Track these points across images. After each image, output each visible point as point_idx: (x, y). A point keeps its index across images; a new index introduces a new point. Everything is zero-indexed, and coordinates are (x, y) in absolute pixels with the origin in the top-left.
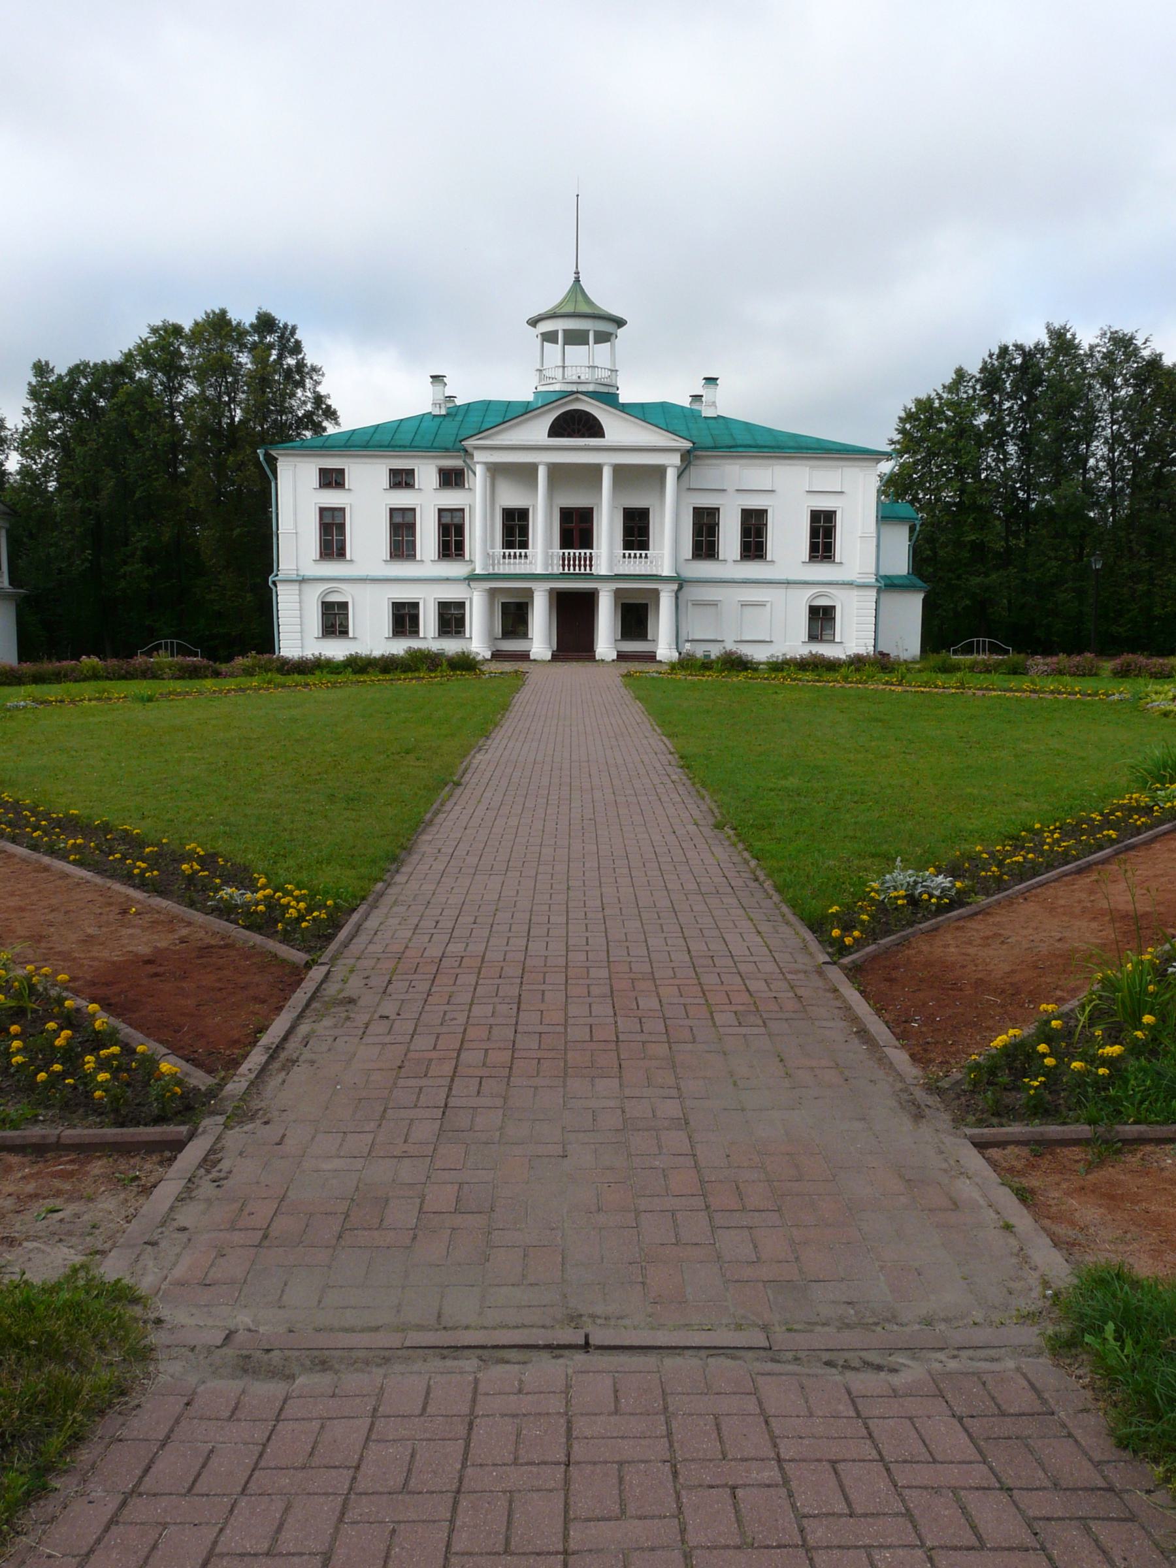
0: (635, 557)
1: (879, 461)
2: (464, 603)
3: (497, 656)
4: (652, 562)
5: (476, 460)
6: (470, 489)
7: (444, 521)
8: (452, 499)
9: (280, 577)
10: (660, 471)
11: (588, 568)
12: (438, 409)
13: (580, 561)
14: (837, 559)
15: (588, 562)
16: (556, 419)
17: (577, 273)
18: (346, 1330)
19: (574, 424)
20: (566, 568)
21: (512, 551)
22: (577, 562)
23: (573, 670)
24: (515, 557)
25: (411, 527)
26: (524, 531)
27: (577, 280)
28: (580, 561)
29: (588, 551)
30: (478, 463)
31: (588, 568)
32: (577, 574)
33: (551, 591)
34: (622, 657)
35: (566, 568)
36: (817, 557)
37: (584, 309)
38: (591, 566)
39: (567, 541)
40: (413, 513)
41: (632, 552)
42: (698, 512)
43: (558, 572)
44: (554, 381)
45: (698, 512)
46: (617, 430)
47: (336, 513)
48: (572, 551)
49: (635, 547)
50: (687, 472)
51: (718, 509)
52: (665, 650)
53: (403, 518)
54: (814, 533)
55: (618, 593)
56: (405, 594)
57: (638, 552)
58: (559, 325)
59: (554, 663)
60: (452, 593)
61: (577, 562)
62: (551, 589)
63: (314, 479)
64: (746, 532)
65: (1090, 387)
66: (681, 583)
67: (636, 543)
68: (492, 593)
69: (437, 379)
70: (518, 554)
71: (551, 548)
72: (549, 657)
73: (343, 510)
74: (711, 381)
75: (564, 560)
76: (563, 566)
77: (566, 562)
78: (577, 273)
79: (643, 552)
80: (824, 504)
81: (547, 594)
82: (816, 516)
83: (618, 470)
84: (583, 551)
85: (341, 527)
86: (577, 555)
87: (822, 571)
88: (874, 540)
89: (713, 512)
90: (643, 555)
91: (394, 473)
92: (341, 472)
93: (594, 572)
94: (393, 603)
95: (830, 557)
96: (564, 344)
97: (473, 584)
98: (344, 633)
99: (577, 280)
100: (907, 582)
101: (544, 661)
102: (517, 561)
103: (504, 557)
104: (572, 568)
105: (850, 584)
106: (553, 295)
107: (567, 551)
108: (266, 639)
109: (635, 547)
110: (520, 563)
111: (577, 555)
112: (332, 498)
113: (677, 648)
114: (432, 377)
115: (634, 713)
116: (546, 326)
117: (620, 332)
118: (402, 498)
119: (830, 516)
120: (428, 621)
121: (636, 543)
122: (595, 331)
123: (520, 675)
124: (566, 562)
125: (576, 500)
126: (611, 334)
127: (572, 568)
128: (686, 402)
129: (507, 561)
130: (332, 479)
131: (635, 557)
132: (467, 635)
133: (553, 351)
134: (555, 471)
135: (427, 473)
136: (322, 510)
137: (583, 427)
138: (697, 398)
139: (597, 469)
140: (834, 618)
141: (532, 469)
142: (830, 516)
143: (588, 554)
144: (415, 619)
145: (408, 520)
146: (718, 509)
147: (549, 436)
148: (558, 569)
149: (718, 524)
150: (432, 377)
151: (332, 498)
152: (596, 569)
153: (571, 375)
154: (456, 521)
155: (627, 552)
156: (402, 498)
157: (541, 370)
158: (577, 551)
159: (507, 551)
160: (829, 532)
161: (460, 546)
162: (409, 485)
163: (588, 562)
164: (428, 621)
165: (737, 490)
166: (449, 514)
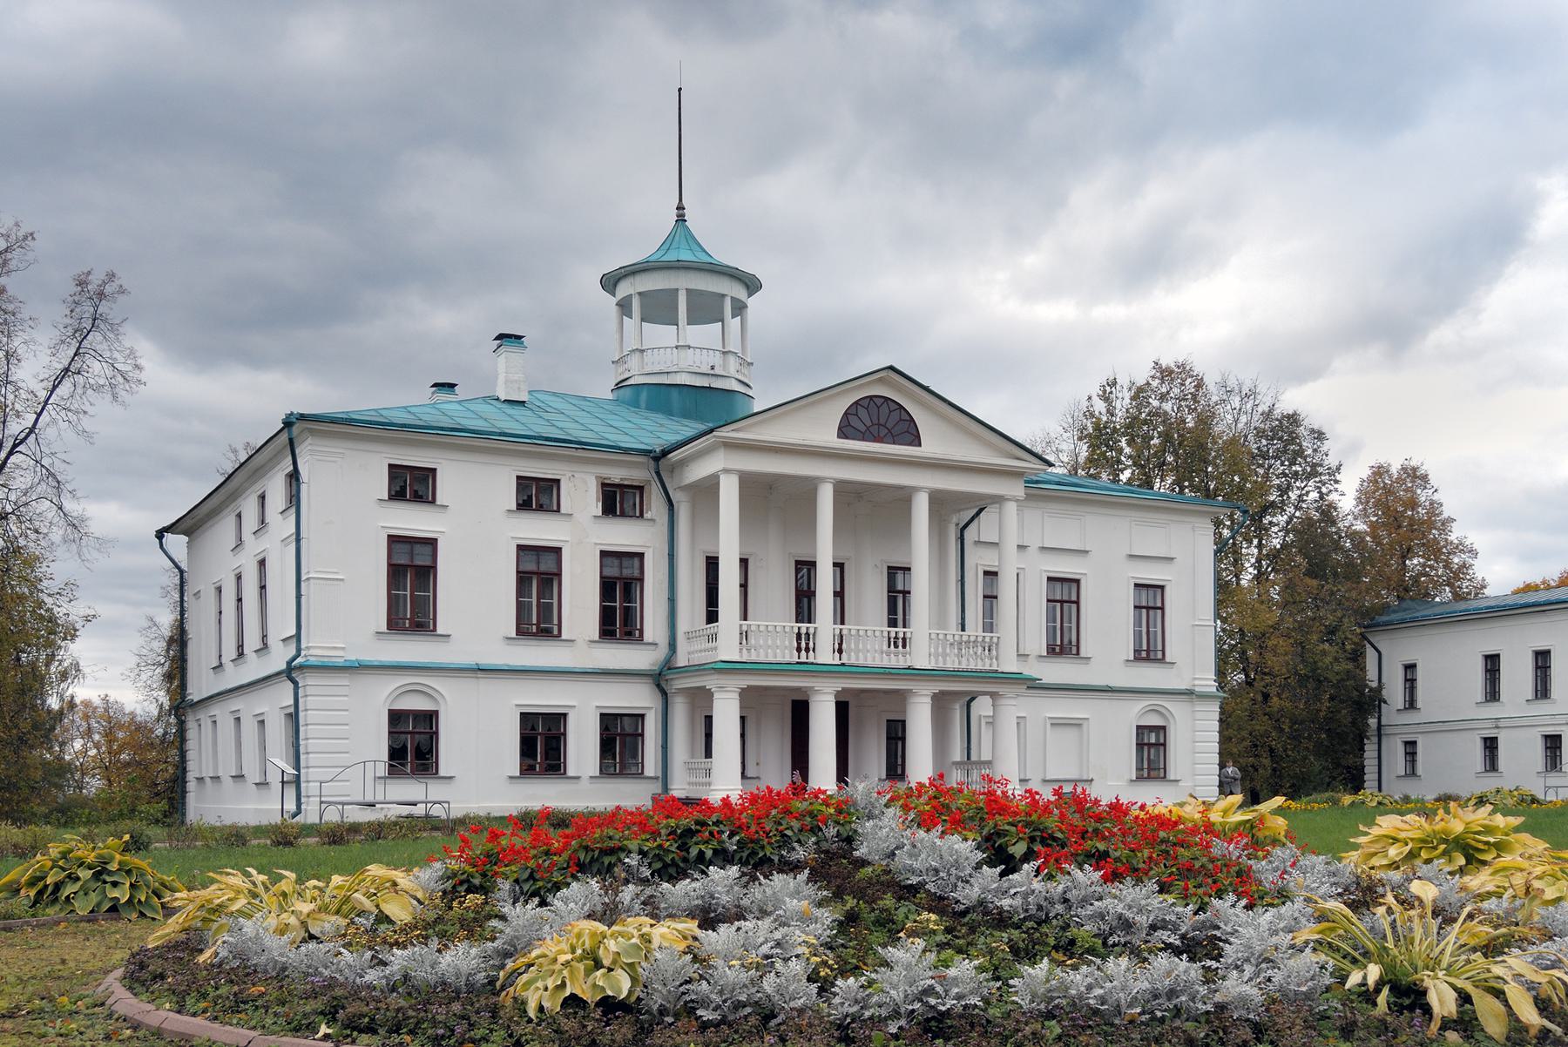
7: (605, 574)
8: (622, 535)
17: (680, 208)
27: (681, 219)
37: (686, 256)
43: (788, 659)
46: (935, 441)
53: (538, 563)
56: (544, 698)
63: (380, 484)
71: (895, 626)
73: (432, 543)
76: (799, 650)
78: (680, 208)
80: (1151, 574)
87: (1148, 676)
91: (523, 482)
99: (681, 219)
105: (1189, 693)
112: (412, 520)
118: (539, 530)
132: (899, 772)
134: (848, 494)
136: (394, 540)
143: (901, 635)
145: (547, 565)
147: (842, 433)
148: (791, 657)
151: (412, 520)
154: (626, 573)
156: (539, 530)
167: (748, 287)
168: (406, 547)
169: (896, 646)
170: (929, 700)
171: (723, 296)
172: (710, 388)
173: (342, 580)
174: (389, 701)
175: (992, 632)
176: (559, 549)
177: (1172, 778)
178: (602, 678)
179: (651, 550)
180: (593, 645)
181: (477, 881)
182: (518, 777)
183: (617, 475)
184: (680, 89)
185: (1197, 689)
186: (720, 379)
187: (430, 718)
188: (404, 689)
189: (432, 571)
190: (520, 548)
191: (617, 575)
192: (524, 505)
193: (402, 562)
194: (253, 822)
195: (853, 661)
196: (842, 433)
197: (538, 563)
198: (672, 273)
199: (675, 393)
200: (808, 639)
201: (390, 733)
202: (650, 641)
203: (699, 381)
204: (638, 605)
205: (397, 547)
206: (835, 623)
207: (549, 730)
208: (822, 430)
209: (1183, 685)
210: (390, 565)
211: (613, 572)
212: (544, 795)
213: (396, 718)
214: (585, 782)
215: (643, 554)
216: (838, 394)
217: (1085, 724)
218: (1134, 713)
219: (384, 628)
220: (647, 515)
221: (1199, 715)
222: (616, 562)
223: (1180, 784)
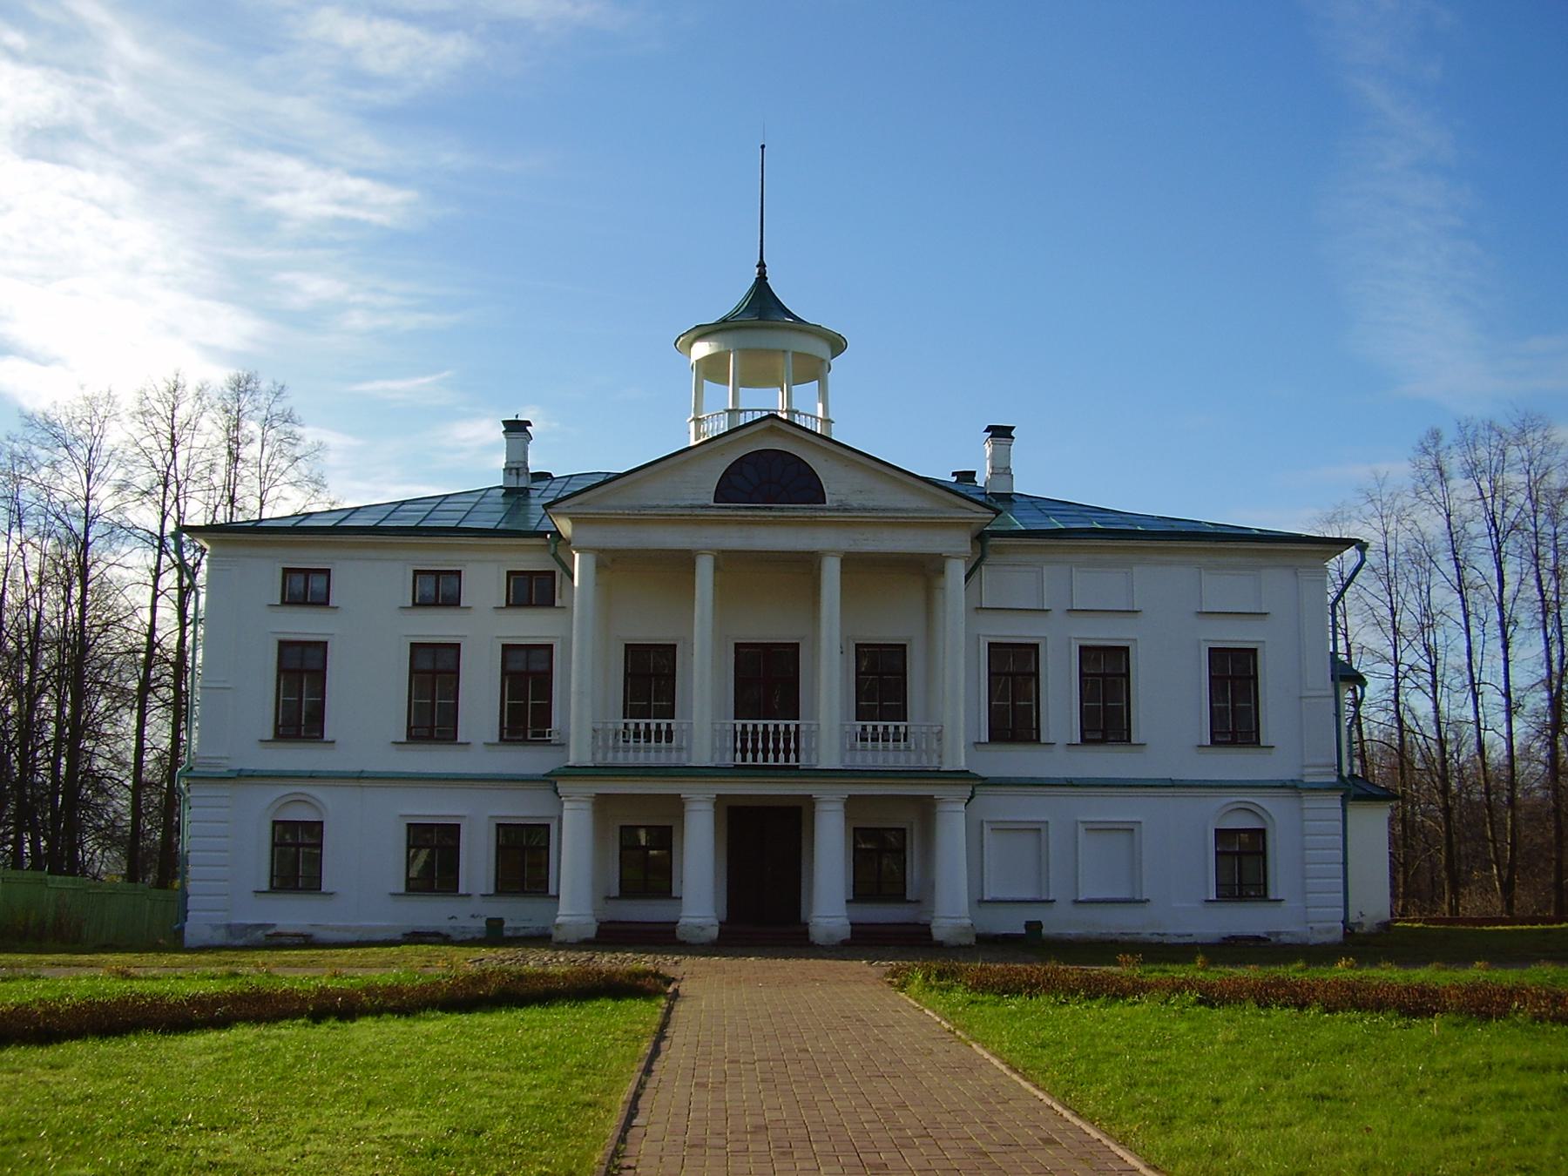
2: (548, 826)
7: (511, 666)
8: (529, 626)
12: (514, 478)
17: (762, 265)
18: (702, 507)
27: (762, 278)
29: (792, 724)
32: (782, 767)
43: (731, 764)
56: (434, 807)
60: (521, 807)
63: (273, 589)
68: (602, 803)
74: (1001, 433)
76: (744, 751)
78: (762, 265)
80: (1234, 635)
85: (320, 674)
87: (1235, 764)
88: (1332, 700)
89: (1029, 652)
93: (803, 762)
97: (564, 787)
98: (313, 885)
99: (762, 278)
105: (1294, 788)
107: (750, 723)
112: (304, 624)
114: (504, 422)
119: (1246, 657)
125: (767, 628)
127: (782, 755)
132: (552, 891)
139: (808, 563)
141: (684, 562)
142: (1246, 657)
151: (304, 624)
152: (809, 758)
156: (436, 626)
161: (544, 716)
162: (453, 601)
166: (522, 654)
169: (658, 740)
170: (840, 806)
173: (229, 688)
175: (906, 720)
176: (551, 646)
177: (1272, 897)
182: (401, 894)
184: (763, 147)
189: (1252, 681)
190: (506, 648)
192: (420, 603)
194: (291, 930)
201: (320, 846)
202: (464, 741)
204: (506, 702)
209: (1287, 774)
211: (518, 665)
215: (459, 645)
218: (1214, 813)
223: (1283, 904)
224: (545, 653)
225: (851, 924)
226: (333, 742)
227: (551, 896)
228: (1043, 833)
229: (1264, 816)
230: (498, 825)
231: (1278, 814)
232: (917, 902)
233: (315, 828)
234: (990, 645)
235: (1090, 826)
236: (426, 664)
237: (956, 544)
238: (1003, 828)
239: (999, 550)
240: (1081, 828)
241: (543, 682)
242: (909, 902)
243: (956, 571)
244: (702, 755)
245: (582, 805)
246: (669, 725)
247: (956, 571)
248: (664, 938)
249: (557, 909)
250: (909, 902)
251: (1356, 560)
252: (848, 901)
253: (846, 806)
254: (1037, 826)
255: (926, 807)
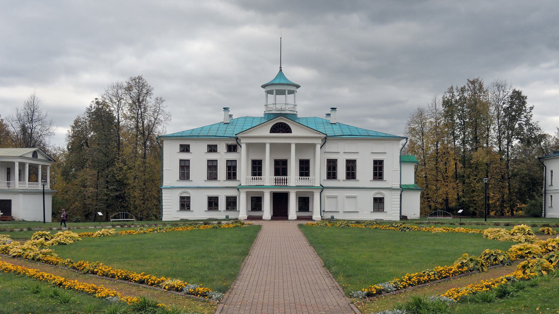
0: (304, 179)
1: (400, 140)
2: (236, 197)
3: (250, 218)
4: (310, 181)
5: (241, 142)
6: (239, 152)
7: (209, 165)
8: (232, 156)
9: (163, 187)
10: (314, 145)
11: (285, 183)
13: (282, 181)
14: (384, 179)
15: (285, 181)
16: (274, 126)
17: (281, 67)
19: (280, 128)
20: (277, 183)
21: (256, 177)
22: (279, 181)
23: (280, 224)
24: (257, 179)
25: (216, 167)
26: (260, 169)
27: (281, 70)
28: (282, 181)
29: (285, 177)
30: (242, 143)
31: (285, 183)
33: (271, 192)
34: (299, 218)
35: (277, 183)
36: (376, 178)
37: (283, 81)
38: (287, 183)
39: (277, 173)
40: (216, 162)
41: (303, 177)
42: (329, 161)
43: (273, 185)
44: (272, 109)
45: (329, 161)
46: (296, 131)
47: (186, 161)
48: (279, 177)
49: (304, 175)
50: (324, 146)
51: (356, 160)
52: (316, 216)
53: (212, 163)
54: (375, 168)
55: (297, 193)
56: (213, 193)
57: (305, 177)
58: (274, 88)
59: (272, 221)
61: (279, 181)
62: (271, 191)
64: (348, 168)
65: (455, 115)
66: (322, 188)
67: (304, 173)
68: (247, 193)
69: (226, 109)
70: (258, 178)
72: (270, 219)
73: (189, 160)
75: (276, 180)
76: (276, 183)
77: (277, 181)
78: (281, 67)
79: (307, 177)
81: (269, 194)
82: (375, 162)
83: (272, 145)
84: (283, 177)
85: (188, 167)
86: (281, 178)
87: (378, 184)
90: (307, 178)
91: (209, 146)
92: (189, 146)
94: (208, 197)
95: (381, 178)
96: (276, 95)
99: (281, 70)
100: (414, 187)
101: (268, 220)
102: (258, 180)
103: (252, 179)
104: (279, 183)
106: (271, 77)
107: (277, 177)
108: (158, 215)
109: (304, 175)
110: (255, 181)
111: (281, 178)
112: (185, 156)
113: (321, 215)
114: (224, 108)
115: (303, 241)
116: (269, 88)
117: (298, 90)
118: (212, 156)
119: (354, 162)
120: (222, 204)
121: (304, 173)
122: (288, 90)
123: (259, 227)
124: (277, 181)
125: (281, 157)
126: (294, 91)
127: (283, 183)
128: (324, 116)
129: (254, 180)
130: (185, 149)
131: (304, 179)
132: (237, 210)
133: (271, 97)
135: (222, 148)
136: (181, 160)
137: (282, 128)
138: (328, 115)
140: (384, 202)
142: (354, 162)
143: (285, 178)
144: (217, 205)
145: (214, 164)
146: (356, 160)
147: (271, 132)
149: (337, 166)
150: (224, 108)
151: (185, 156)
153: (278, 107)
155: (301, 177)
156: (212, 156)
157: (267, 105)
158: (281, 177)
159: (254, 177)
160: (381, 168)
161: (235, 174)
163: (285, 181)
164: (222, 204)
165: (372, 153)
167: (297, 87)
168: (184, 162)
171: (285, 90)
172: (281, 113)
174: (179, 195)
176: (217, 160)
178: (231, 189)
179: (238, 159)
180: (225, 181)
181: (528, 255)
183: (230, 143)
184: (281, 38)
185: (393, 187)
186: (283, 111)
187: (189, 198)
188: (183, 192)
190: (208, 161)
191: (231, 165)
193: (183, 165)
195: (289, 185)
196: (271, 132)
197: (212, 163)
198: (272, 86)
199: (272, 115)
200: (278, 180)
203: (278, 112)
205: (182, 162)
206: (270, 176)
207: (210, 200)
208: (266, 131)
210: (180, 166)
211: (229, 164)
212: (213, 215)
213: (182, 198)
214: (222, 212)
216: (265, 124)
217: (357, 197)
218: (371, 195)
219: (179, 179)
220: (238, 151)
221: (393, 194)
222: (231, 162)
224: (235, 162)
225: (297, 216)
226: (192, 180)
227: (238, 211)
228: (337, 199)
229: (384, 194)
230: (226, 197)
231: (193, 194)
232: (311, 212)
233: (189, 198)
234: (327, 159)
235: (347, 197)
236: (211, 164)
237: (319, 142)
238: (329, 197)
239: (329, 140)
240: (345, 197)
241: (235, 168)
242: (310, 212)
243: (318, 147)
244: (267, 183)
245: (244, 193)
246: (261, 178)
247: (318, 147)
248: (260, 218)
249: (239, 213)
250: (310, 212)
251: (406, 142)
252: (296, 212)
253: (296, 193)
254: (336, 197)
255: (312, 193)
